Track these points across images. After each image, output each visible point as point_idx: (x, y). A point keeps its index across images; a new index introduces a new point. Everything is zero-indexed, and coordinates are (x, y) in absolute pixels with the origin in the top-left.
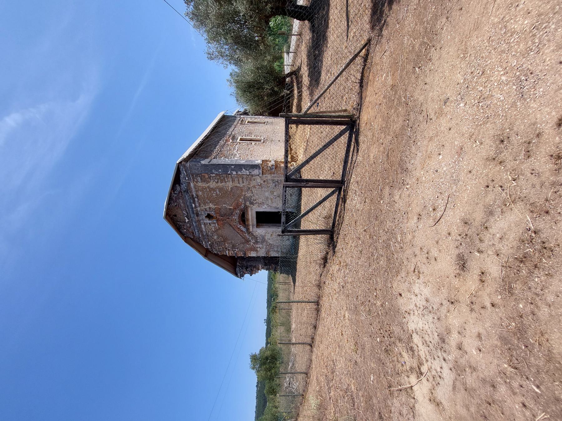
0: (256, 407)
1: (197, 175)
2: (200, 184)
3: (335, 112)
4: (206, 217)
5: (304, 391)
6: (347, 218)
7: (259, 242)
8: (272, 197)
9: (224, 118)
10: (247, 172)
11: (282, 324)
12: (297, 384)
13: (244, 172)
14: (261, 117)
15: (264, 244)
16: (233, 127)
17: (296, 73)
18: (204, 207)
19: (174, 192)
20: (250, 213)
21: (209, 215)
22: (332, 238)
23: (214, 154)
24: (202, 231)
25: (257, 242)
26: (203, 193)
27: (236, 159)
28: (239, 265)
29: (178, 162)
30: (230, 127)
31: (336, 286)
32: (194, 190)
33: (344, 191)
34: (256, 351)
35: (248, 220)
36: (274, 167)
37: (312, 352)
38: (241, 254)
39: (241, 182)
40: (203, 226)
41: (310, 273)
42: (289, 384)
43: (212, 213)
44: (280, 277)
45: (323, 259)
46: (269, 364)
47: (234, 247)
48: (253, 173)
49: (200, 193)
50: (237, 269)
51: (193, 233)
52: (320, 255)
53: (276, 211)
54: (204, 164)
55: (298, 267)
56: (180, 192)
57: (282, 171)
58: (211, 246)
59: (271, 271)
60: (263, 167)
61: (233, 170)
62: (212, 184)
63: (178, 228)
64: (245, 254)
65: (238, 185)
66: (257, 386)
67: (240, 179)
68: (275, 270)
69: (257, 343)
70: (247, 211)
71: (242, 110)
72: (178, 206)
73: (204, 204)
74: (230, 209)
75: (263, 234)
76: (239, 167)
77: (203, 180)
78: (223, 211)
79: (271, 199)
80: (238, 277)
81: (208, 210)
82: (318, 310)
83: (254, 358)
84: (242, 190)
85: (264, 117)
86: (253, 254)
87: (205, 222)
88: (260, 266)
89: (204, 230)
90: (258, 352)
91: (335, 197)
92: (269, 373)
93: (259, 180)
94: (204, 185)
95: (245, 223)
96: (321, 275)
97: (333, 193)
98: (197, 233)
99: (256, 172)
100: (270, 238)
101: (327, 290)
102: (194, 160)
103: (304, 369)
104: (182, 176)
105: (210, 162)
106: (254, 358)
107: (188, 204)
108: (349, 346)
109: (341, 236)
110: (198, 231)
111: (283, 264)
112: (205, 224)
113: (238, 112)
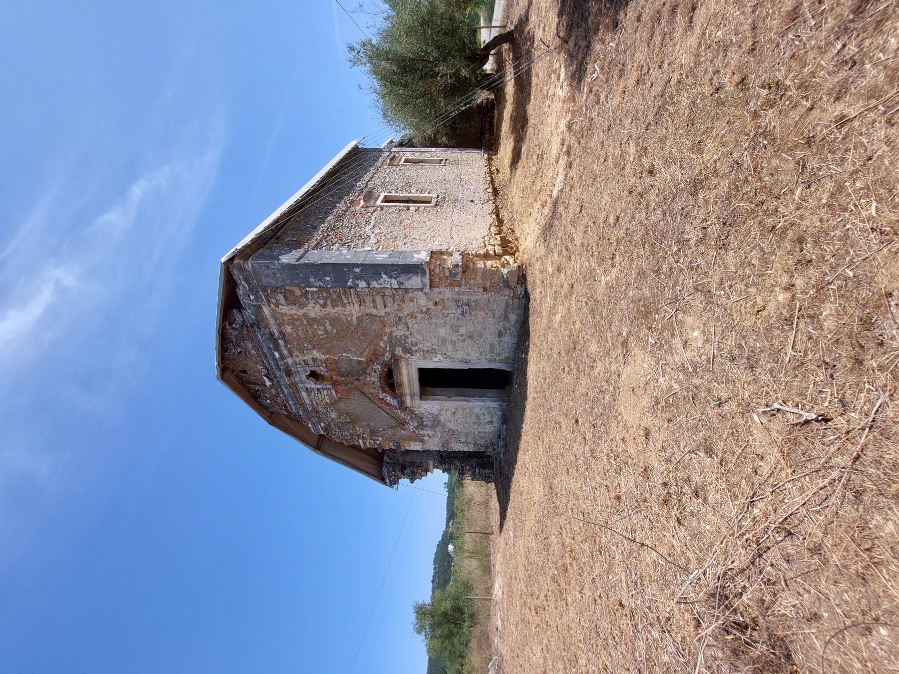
1: (275, 289)
7: (426, 426)
9: (356, 153)
10: (394, 281)
11: (474, 554)
13: (387, 282)
14: (433, 149)
16: (372, 170)
17: (515, 39)
18: (300, 358)
19: (231, 324)
20: (404, 372)
23: (317, 237)
24: (303, 404)
25: (422, 426)
26: (296, 328)
27: (367, 248)
28: (389, 464)
29: (223, 260)
30: (366, 171)
35: (401, 385)
36: (460, 270)
38: (391, 445)
39: (380, 304)
40: (304, 394)
43: (322, 370)
44: (473, 488)
47: (373, 433)
48: (408, 285)
49: (289, 329)
50: (385, 470)
51: (285, 406)
53: (465, 367)
54: (288, 265)
60: (432, 271)
61: (357, 277)
62: (313, 310)
65: (374, 312)
66: (433, 581)
67: (379, 299)
68: (462, 474)
69: (423, 591)
71: (397, 139)
72: (245, 353)
74: (360, 362)
76: (373, 270)
77: (291, 300)
79: (454, 343)
80: (385, 484)
81: (311, 362)
85: (439, 150)
86: (415, 446)
87: (308, 386)
89: (307, 402)
93: (423, 301)
94: (294, 311)
95: (394, 391)
99: (415, 281)
104: (240, 292)
105: (301, 257)
106: (421, 611)
107: (265, 350)
110: (294, 404)
113: (392, 142)
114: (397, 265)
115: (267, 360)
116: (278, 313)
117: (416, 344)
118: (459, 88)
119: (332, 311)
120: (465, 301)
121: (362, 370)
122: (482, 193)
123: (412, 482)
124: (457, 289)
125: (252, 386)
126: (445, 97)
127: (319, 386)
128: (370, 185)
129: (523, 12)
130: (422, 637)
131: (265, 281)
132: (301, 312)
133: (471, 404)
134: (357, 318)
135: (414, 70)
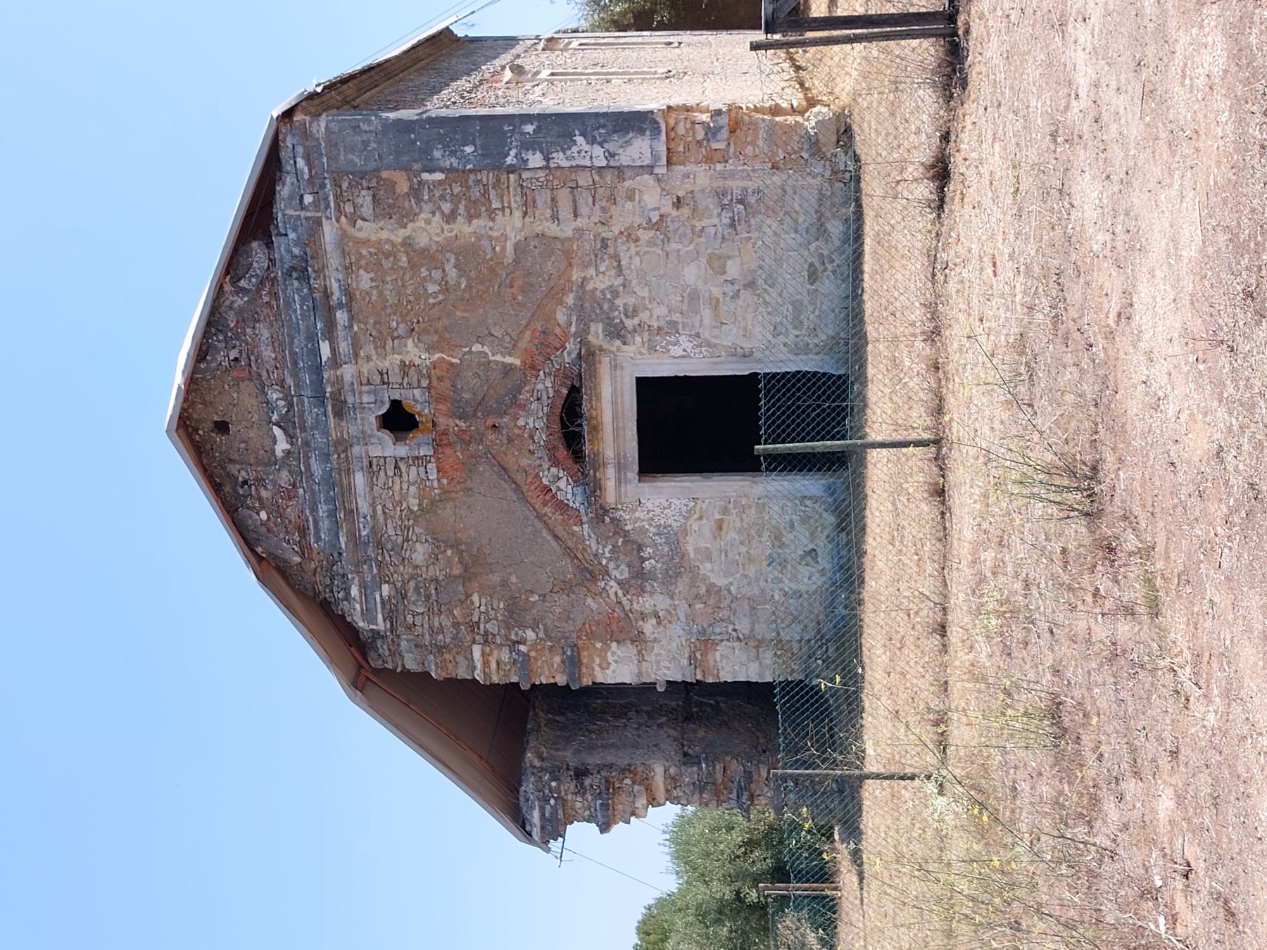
2: (367, 230)
3: (571, 81)
8: (716, 292)
10: (598, 151)
13: (585, 152)
15: (681, 586)
19: (234, 282)
20: (606, 390)
25: (639, 579)
26: (380, 279)
32: (334, 260)
38: (550, 671)
40: (359, 479)
43: (416, 400)
47: (515, 613)
48: (624, 158)
50: (529, 786)
51: (303, 531)
53: (742, 370)
56: (267, 279)
61: (529, 145)
62: (427, 229)
64: (574, 663)
65: (552, 229)
67: (564, 196)
70: (594, 374)
72: (246, 368)
73: (380, 346)
74: (508, 370)
76: (561, 127)
77: (387, 208)
79: (715, 304)
80: (527, 836)
81: (395, 378)
84: (568, 254)
86: (616, 667)
87: (375, 451)
88: (659, 770)
89: (364, 506)
98: (325, 524)
99: (638, 150)
110: (333, 514)
112: (372, 468)
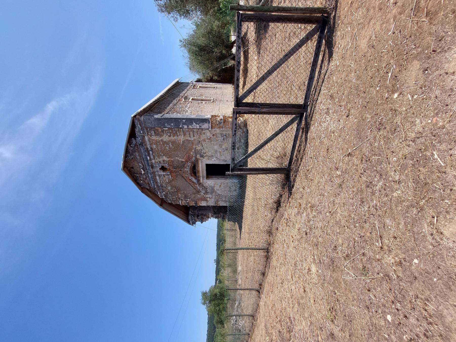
0: (208, 331)
1: (151, 129)
4: (161, 169)
5: (250, 331)
6: (310, 151)
8: (220, 150)
9: (178, 84)
10: (198, 126)
11: (229, 266)
12: (243, 323)
13: (195, 126)
16: (186, 90)
19: (130, 145)
20: (200, 166)
21: (163, 167)
22: (288, 177)
23: (167, 110)
24: (157, 182)
25: (206, 193)
26: (157, 146)
28: (191, 213)
29: (132, 116)
31: (295, 232)
32: (148, 143)
33: (306, 119)
34: (207, 289)
35: (199, 172)
36: (222, 121)
37: (259, 297)
38: (192, 204)
39: (192, 136)
40: (158, 178)
41: (258, 220)
42: (236, 321)
43: (166, 165)
44: (228, 224)
45: (276, 203)
46: (218, 301)
47: (186, 197)
48: (203, 127)
49: (154, 146)
50: (190, 217)
51: (149, 184)
52: (275, 198)
53: (225, 163)
55: (244, 215)
56: (136, 145)
57: (230, 126)
58: (165, 196)
59: (220, 219)
60: (212, 122)
61: (184, 124)
62: (165, 138)
63: (136, 180)
65: (189, 139)
67: (191, 133)
68: (223, 219)
69: (208, 282)
70: (198, 163)
72: (135, 159)
75: (212, 185)
76: (190, 121)
77: (157, 134)
78: (176, 164)
79: (220, 152)
80: (190, 224)
81: (162, 162)
82: (267, 258)
83: (204, 294)
84: (193, 143)
86: (203, 204)
87: (160, 173)
88: (210, 214)
89: (159, 181)
90: (208, 290)
91: (295, 126)
92: (218, 308)
93: (208, 134)
95: (196, 175)
96: (273, 220)
97: (292, 121)
99: (206, 126)
100: (219, 190)
101: (279, 237)
102: (149, 114)
103: (249, 312)
104: (137, 130)
106: (204, 294)
108: (320, 311)
109: (301, 173)
110: (153, 182)
111: (231, 212)
114: (199, 119)
115: (144, 161)
116: (150, 139)
117: (205, 153)
118: (222, 57)
119: (173, 138)
120: (225, 134)
121: (183, 165)
122: (231, 98)
123: (202, 223)
124: (221, 129)
125: (135, 175)
126: (217, 61)
127: (164, 174)
128: (186, 95)
129: (246, 31)
130: (205, 307)
131: (148, 125)
132: (160, 139)
133: (227, 181)
134: (183, 141)
135: (204, 50)
